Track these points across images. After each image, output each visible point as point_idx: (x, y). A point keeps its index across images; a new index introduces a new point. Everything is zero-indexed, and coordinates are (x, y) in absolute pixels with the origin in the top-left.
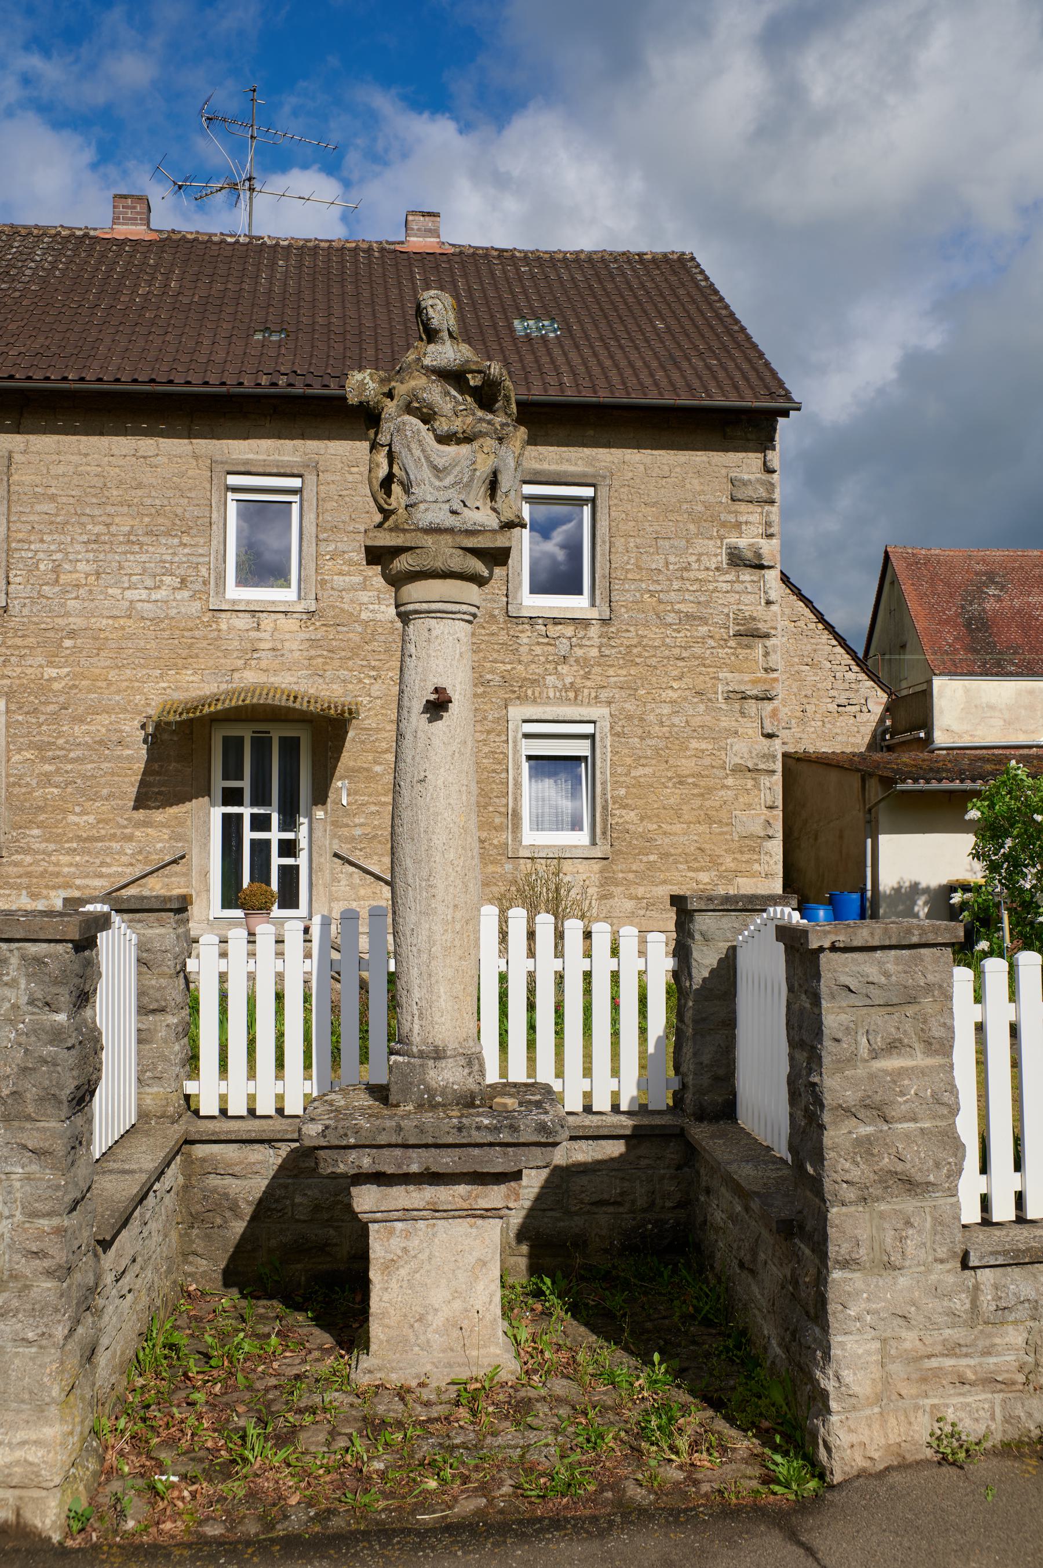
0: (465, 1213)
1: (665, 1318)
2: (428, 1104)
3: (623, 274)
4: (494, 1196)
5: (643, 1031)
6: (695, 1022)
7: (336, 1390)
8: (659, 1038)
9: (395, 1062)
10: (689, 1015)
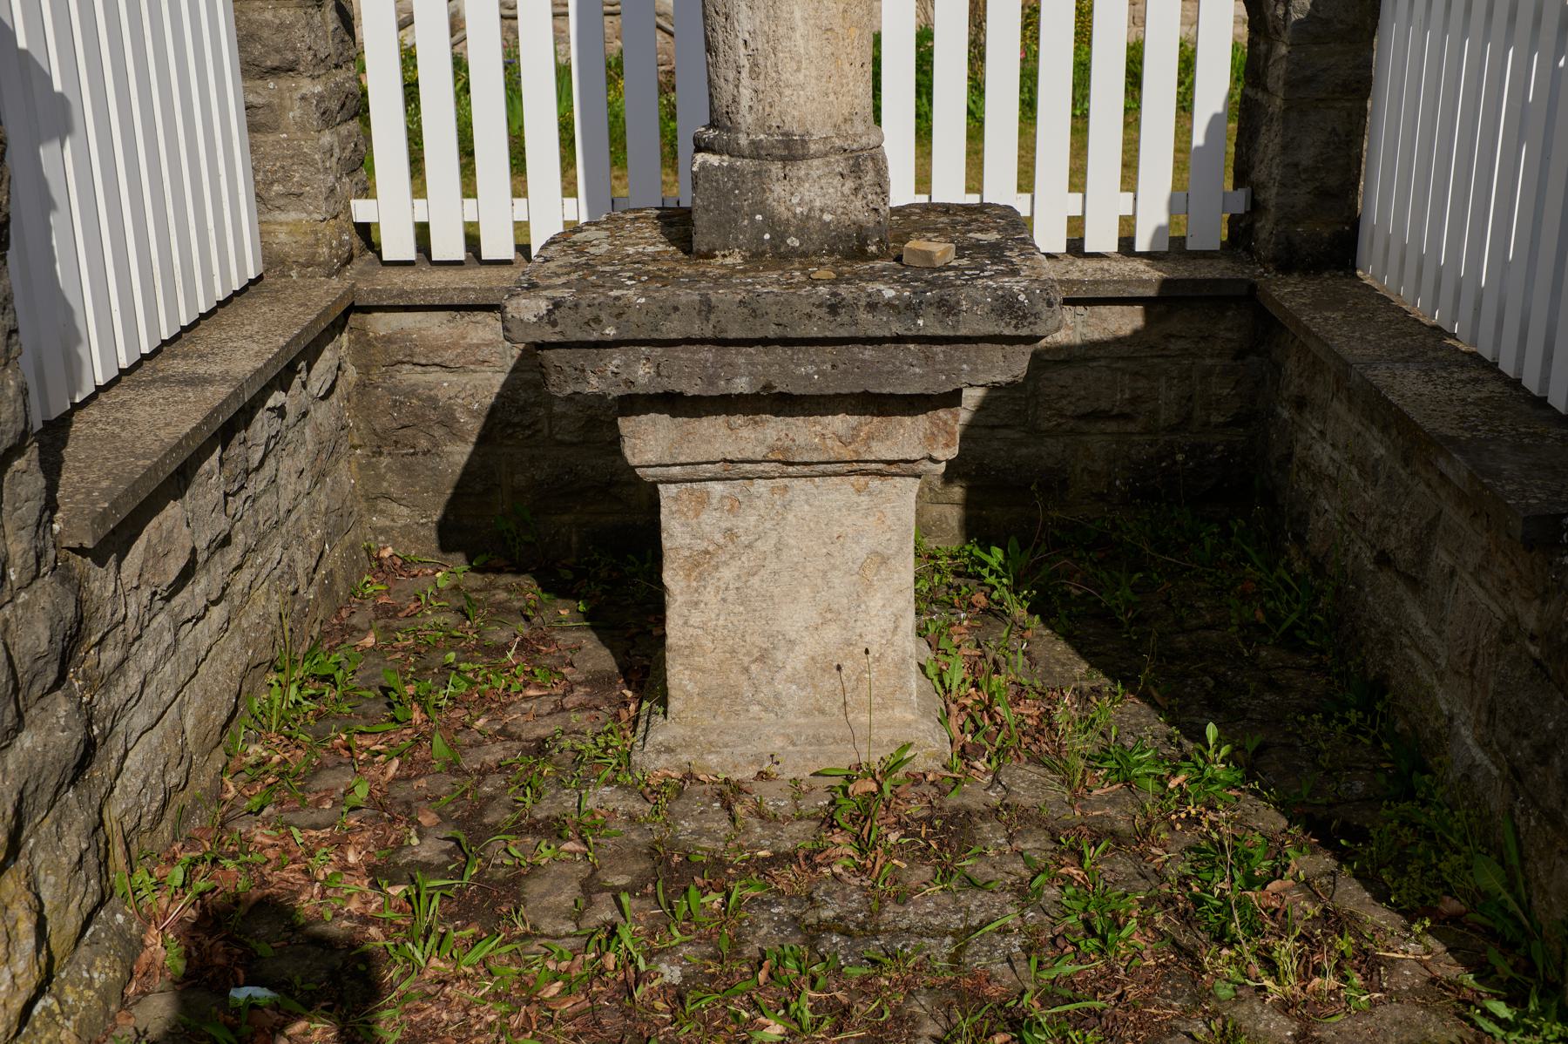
0: (847, 467)
1: (1209, 627)
2: (772, 252)
4: (906, 437)
5: (1185, 105)
6: (1290, 85)
7: (608, 783)
8: (1215, 117)
9: (703, 166)
10: (1276, 74)
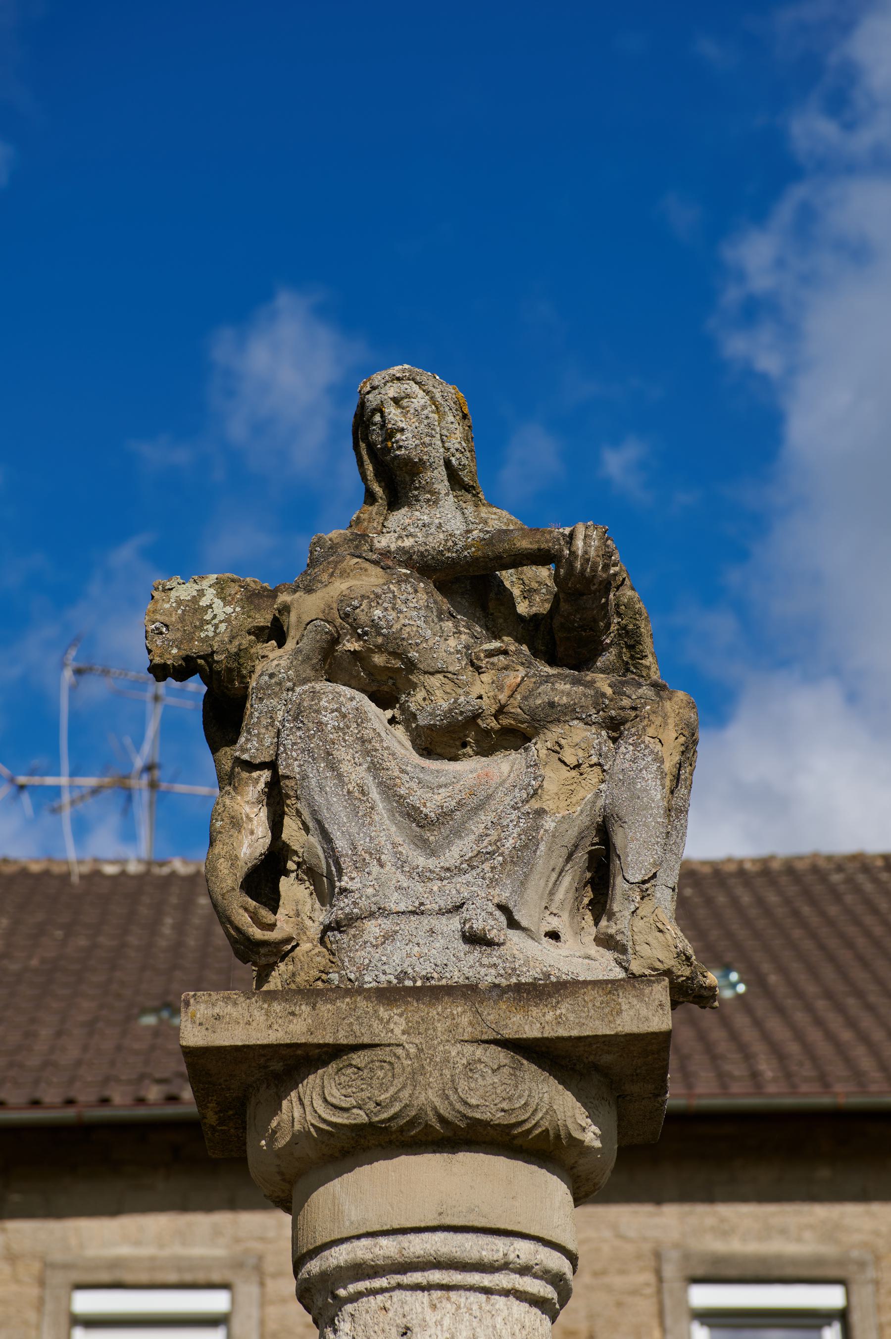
3: (857, 889)
